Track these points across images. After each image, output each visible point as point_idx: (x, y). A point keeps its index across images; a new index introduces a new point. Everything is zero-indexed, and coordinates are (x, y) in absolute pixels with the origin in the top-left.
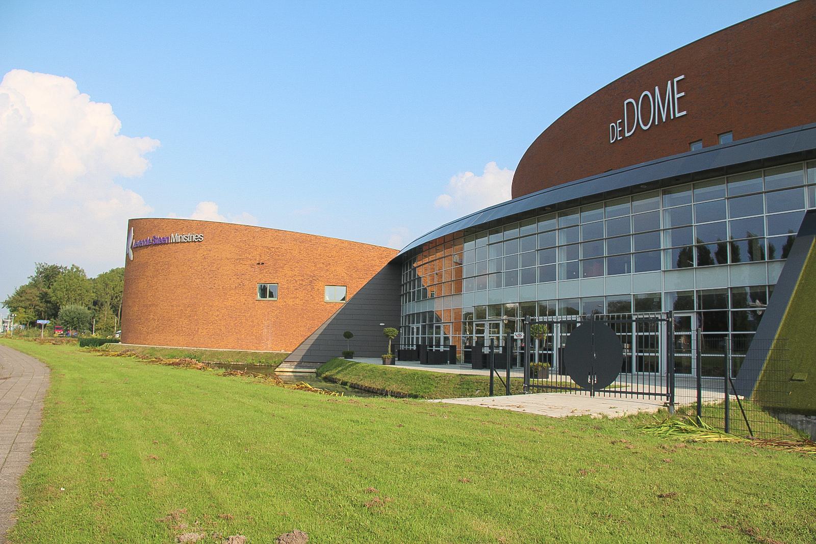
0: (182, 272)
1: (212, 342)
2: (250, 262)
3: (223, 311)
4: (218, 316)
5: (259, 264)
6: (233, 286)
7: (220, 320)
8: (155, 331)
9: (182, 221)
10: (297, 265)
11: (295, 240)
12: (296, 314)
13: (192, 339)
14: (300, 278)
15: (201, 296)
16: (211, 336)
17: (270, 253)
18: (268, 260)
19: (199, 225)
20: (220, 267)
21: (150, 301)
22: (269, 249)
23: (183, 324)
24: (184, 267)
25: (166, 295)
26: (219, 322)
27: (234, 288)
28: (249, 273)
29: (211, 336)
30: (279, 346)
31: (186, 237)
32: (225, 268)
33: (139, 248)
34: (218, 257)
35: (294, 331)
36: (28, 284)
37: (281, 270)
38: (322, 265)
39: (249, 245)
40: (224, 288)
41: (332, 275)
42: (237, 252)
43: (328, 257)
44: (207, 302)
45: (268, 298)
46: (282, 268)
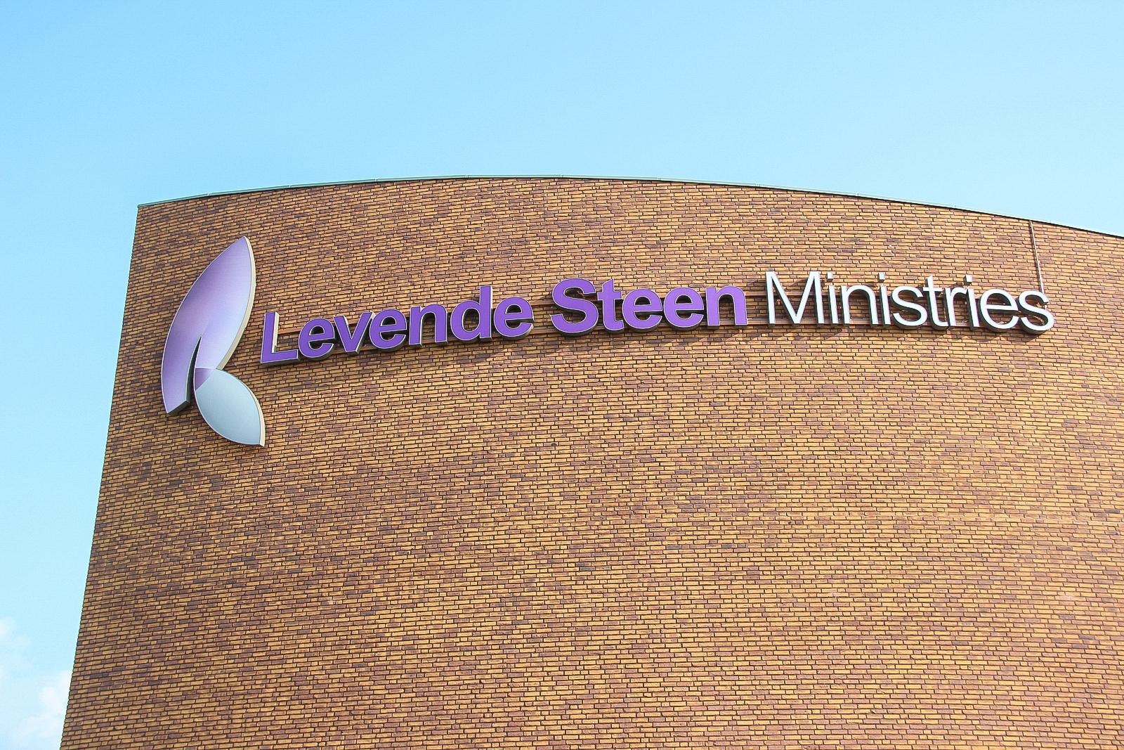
0: (902, 526)
9: (838, 206)
33: (352, 365)
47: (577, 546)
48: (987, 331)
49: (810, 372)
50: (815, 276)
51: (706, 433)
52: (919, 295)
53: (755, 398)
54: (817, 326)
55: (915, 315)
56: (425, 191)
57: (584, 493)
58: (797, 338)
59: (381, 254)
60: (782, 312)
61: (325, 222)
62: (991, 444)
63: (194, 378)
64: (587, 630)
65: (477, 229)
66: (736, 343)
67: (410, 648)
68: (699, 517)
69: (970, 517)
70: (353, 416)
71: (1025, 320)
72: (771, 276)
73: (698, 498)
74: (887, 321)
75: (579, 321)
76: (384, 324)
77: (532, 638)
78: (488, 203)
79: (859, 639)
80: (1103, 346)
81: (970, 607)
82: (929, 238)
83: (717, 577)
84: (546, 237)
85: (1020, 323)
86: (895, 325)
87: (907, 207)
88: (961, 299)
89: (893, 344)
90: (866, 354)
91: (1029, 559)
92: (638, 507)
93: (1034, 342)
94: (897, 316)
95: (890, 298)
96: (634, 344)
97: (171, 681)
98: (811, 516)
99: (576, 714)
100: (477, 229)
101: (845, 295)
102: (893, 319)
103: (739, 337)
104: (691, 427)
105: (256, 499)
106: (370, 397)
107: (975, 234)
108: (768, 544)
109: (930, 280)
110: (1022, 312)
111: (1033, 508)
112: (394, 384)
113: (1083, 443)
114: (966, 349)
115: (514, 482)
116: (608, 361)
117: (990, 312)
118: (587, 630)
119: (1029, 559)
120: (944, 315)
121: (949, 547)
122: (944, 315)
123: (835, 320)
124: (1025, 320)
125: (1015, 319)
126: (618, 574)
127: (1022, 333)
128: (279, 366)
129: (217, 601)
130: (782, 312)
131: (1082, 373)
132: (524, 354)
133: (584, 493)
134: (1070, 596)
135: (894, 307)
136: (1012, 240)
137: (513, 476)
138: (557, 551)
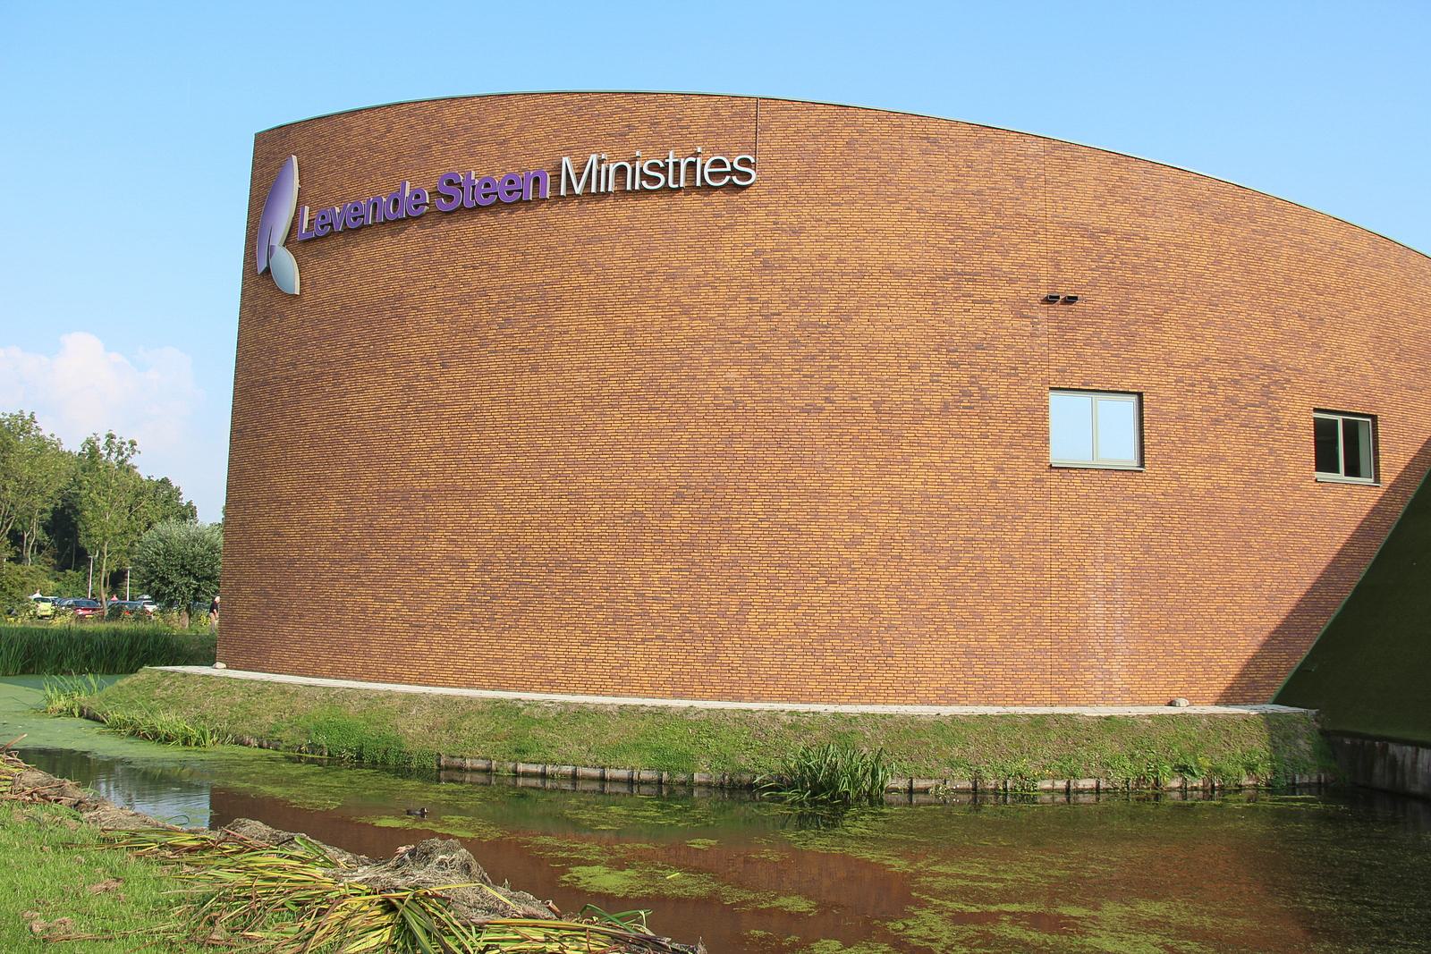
0: (630, 331)
1: (827, 670)
2: (1007, 291)
3: (882, 521)
4: (855, 542)
5: (1051, 300)
6: (933, 401)
7: (870, 562)
8: (466, 615)
9: (620, 101)
10: (1210, 315)
11: (1196, 205)
12: (1221, 533)
13: (710, 659)
14: (1227, 373)
15: (756, 446)
16: (822, 639)
17: (1101, 258)
18: (1093, 284)
19: (725, 113)
20: (857, 310)
21: (424, 474)
22: (1092, 236)
23: (644, 583)
24: (644, 309)
25: (532, 445)
26: (867, 571)
27: (935, 408)
28: (1009, 341)
29: (822, 639)
30: (1162, 682)
31: (653, 167)
32: (884, 314)
33: (341, 240)
34: (840, 261)
35: (1218, 610)
36: (223, 517)
37: (1149, 333)
38: (1295, 323)
39: (998, 213)
40: (885, 407)
41: (1332, 367)
42: (943, 243)
43: (1313, 288)
44: (792, 476)
45: (1340, 476)
46: (1155, 322)
47: (443, 353)
48: (707, 189)
49: (586, 227)
50: (594, 158)
51: (519, 274)
52: (662, 165)
53: (549, 248)
54: (625, 192)
55: (657, 180)
56: (381, 114)
57: (448, 318)
58: (580, 204)
59: (358, 161)
60: (569, 185)
61: (333, 140)
62: (698, 271)
63: (271, 249)
64: (443, 405)
65: (406, 140)
66: (542, 210)
67: (360, 417)
68: (508, 331)
69: (675, 324)
70: (340, 272)
71: (734, 178)
72: (566, 160)
73: (509, 319)
74: (637, 187)
75: (455, 204)
76: (509, 184)
77: (417, 411)
78: (413, 121)
79: (592, 408)
80: (796, 191)
81: (665, 386)
82: (680, 120)
83: (515, 371)
84: (441, 142)
85: (731, 180)
86: (642, 189)
87: (670, 97)
88: (692, 165)
89: (643, 203)
90: (621, 212)
91: (709, 351)
92: (475, 326)
93: (744, 193)
94: (644, 183)
95: (641, 169)
96: (482, 216)
97: (264, 435)
98: (573, 328)
99: (435, 456)
100: (406, 140)
101: (612, 169)
102: (641, 185)
103: (545, 205)
104: (511, 270)
105: (297, 327)
106: (348, 260)
107: (716, 113)
108: (546, 347)
109: (671, 153)
110: (734, 171)
111: (719, 315)
112: (361, 252)
113: (766, 265)
114: (692, 202)
115: (413, 313)
116: (468, 228)
117: (710, 174)
118: (443, 405)
119: (709, 351)
120: (677, 180)
121: (658, 345)
122: (677, 180)
123: (602, 190)
124: (734, 178)
125: (728, 178)
126: (463, 369)
127: (732, 187)
128: (309, 240)
129: (279, 390)
130: (569, 185)
131: (776, 214)
132: (423, 227)
133: (448, 318)
134: (733, 375)
135: (644, 176)
136: (743, 114)
137: (413, 308)
138: (431, 357)
